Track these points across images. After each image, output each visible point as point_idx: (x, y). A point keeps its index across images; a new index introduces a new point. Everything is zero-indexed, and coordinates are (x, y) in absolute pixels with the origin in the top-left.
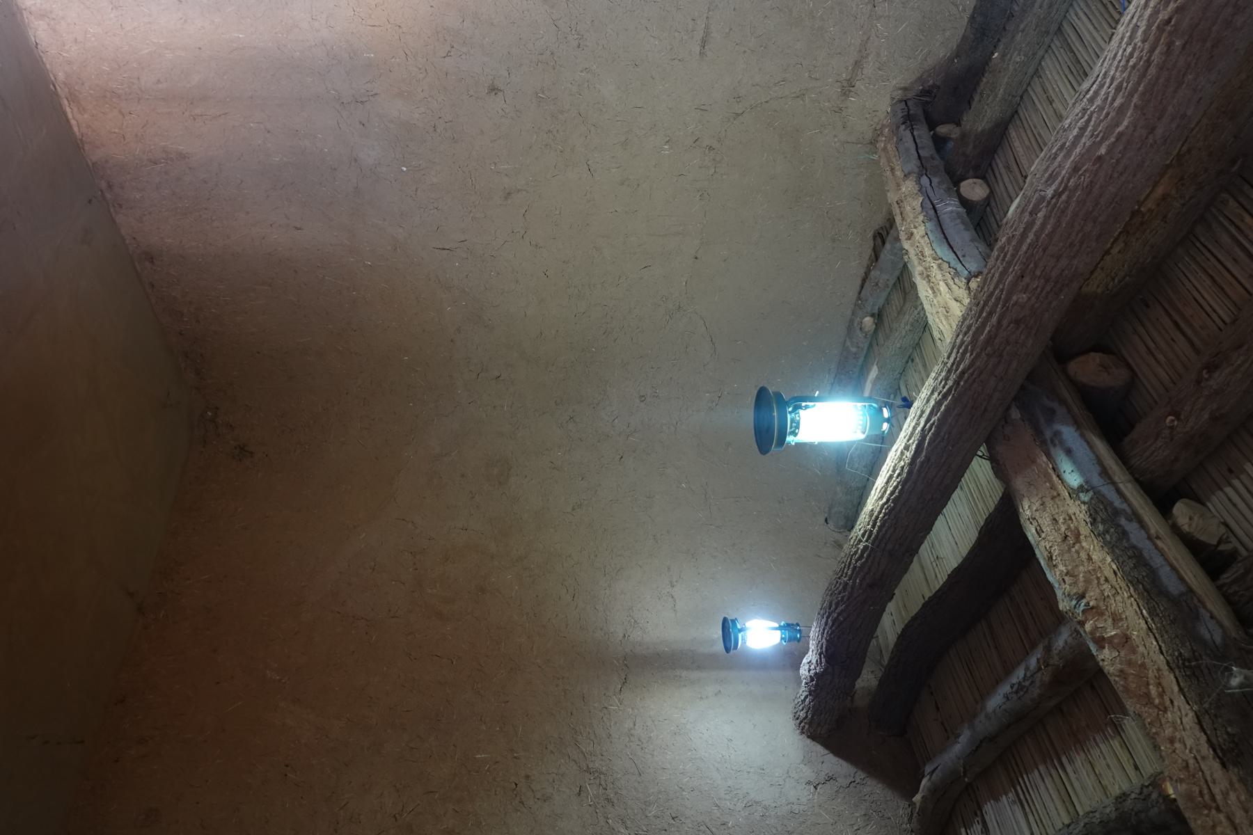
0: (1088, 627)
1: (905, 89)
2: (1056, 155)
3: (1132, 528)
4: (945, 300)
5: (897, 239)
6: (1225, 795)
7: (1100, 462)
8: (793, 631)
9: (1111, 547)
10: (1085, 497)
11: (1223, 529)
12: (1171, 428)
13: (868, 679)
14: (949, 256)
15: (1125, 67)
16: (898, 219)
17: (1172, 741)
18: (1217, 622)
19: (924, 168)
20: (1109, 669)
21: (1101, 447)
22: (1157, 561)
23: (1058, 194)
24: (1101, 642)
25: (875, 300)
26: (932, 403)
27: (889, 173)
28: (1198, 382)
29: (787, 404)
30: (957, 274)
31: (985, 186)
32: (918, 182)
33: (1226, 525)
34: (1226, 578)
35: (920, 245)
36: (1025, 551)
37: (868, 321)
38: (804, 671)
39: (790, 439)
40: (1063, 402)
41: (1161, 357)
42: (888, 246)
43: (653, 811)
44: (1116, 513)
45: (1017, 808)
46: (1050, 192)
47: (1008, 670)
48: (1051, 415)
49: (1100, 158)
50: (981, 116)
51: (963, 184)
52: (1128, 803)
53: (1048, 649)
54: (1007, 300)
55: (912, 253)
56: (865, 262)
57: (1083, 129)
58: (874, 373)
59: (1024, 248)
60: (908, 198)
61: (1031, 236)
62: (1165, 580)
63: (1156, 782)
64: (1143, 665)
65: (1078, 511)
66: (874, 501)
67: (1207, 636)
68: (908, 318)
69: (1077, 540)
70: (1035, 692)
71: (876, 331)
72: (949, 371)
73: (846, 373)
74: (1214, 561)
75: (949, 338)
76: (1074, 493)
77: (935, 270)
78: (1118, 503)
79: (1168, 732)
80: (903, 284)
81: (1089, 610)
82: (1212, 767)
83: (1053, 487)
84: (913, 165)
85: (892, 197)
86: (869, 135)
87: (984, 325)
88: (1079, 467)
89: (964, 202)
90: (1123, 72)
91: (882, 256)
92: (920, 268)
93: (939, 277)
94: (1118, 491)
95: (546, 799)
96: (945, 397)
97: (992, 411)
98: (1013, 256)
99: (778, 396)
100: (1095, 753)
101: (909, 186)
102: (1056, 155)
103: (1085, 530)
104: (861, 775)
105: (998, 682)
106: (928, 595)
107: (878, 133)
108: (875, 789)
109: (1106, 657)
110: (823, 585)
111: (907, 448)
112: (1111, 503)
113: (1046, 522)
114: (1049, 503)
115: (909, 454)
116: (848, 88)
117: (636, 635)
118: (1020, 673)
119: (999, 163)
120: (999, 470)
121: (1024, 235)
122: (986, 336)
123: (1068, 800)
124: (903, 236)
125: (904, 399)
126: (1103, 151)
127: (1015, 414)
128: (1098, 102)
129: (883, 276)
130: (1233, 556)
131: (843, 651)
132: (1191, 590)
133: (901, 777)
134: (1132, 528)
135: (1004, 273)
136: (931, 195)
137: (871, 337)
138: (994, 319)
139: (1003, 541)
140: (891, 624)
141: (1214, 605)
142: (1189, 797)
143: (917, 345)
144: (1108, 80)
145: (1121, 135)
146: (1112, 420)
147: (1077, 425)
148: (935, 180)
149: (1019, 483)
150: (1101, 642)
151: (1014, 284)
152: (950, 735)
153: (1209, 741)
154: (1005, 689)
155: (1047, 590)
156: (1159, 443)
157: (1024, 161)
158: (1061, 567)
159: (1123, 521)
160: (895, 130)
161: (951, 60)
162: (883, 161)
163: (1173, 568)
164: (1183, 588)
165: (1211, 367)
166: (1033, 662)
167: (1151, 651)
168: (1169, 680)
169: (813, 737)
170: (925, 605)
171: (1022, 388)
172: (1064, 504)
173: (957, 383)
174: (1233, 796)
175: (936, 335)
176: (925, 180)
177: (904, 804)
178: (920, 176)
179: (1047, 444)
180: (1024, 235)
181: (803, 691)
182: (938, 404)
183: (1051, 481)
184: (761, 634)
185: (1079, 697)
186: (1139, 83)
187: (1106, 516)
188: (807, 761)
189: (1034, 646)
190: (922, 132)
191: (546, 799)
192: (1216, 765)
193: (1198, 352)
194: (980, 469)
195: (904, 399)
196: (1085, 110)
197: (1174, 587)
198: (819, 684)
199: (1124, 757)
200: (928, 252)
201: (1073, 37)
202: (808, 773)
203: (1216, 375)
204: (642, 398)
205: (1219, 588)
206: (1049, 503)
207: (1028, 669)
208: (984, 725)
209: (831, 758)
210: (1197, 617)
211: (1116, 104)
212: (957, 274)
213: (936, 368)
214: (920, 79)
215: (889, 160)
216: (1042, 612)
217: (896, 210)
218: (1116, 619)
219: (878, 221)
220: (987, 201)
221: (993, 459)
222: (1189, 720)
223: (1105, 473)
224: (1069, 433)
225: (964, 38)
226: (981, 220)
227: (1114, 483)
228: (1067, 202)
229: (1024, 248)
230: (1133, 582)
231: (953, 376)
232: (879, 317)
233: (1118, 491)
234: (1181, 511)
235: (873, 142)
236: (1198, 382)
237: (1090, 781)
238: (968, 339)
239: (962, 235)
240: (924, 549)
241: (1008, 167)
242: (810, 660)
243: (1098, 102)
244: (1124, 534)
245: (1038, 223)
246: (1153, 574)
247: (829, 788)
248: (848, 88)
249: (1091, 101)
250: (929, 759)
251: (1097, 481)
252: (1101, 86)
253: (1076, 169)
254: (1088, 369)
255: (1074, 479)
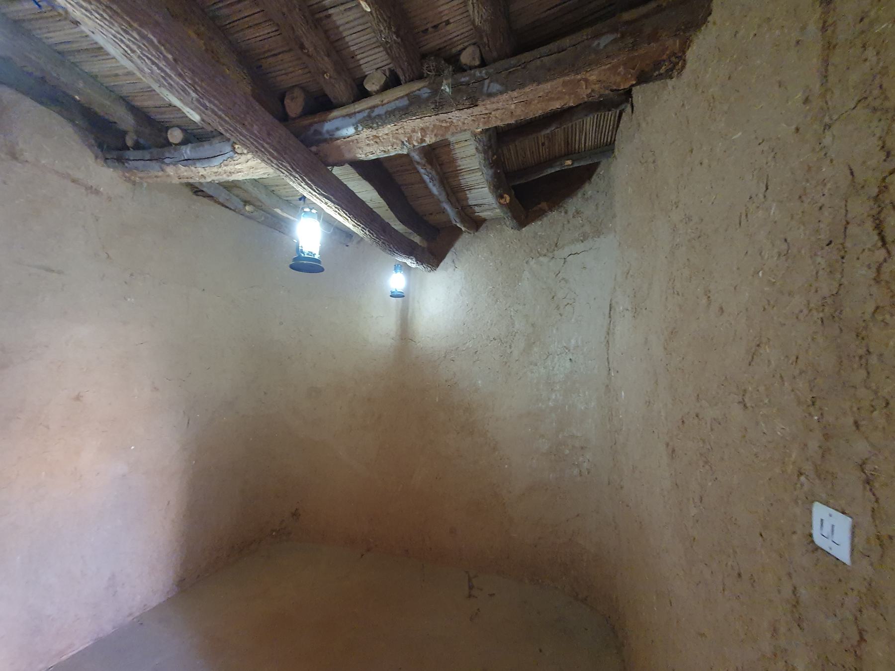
0: (416, 144)
1: (96, 157)
2: (169, 84)
3: (377, 112)
4: (247, 166)
5: (201, 183)
6: (486, 109)
7: (344, 116)
8: (396, 268)
9: (384, 124)
10: (360, 128)
11: (379, 71)
12: (330, 77)
13: (417, 239)
14: (219, 160)
15: (112, 23)
16: (191, 181)
17: (464, 123)
18: (420, 88)
19: (160, 159)
20: (433, 140)
21: (335, 113)
22: (393, 106)
23: (196, 91)
24: (423, 141)
25: (236, 202)
26: (306, 187)
27: (159, 179)
28: (309, 56)
29: (300, 256)
30: (232, 157)
31: (174, 129)
32: (168, 165)
33: (377, 69)
34: (402, 78)
35: (209, 173)
36: (377, 162)
37: (247, 208)
38: (414, 266)
39: (317, 257)
40: (311, 125)
41: (291, 69)
42: (204, 189)
43: (461, 332)
44: (369, 116)
45: (473, 191)
46: (194, 95)
47: (424, 182)
48: (317, 132)
49: (175, 60)
50: (126, 121)
51: (171, 140)
52: (480, 148)
53: (418, 163)
54: (256, 136)
55: (214, 178)
56: (212, 203)
57: (153, 63)
58: (278, 211)
59: (227, 119)
60: (176, 173)
61: (220, 113)
62: (401, 105)
63: (475, 135)
64: (434, 126)
65: (366, 133)
66: (349, 224)
67: (427, 95)
68: (250, 188)
69: (378, 137)
70: (434, 173)
71: (254, 205)
72: (291, 175)
73: (279, 226)
74: (393, 82)
75: (270, 170)
76: (357, 133)
77: (228, 169)
78: (365, 114)
79: (460, 123)
80: (230, 186)
81: (409, 141)
82: (476, 111)
83: (353, 141)
84: (155, 164)
85: (176, 181)
86: (130, 185)
87: (269, 152)
88: (347, 126)
89: (185, 142)
90: (113, 25)
91: (211, 194)
92: (225, 176)
93: (232, 167)
94: (359, 112)
95: (455, 374)
96: (304, 180)
97: (313, 158)
98: (231, 126)
99: (295, 259)
100: (458, 155)
101: (170, 170)
102: (169, 84)
103: (374, 133)
104: (452, 249)
105: (427, 187)
106: (387, 207)
107: (128, 180)
108: (458, 245)
109: (429, 140)
110: (378, 250)
111: (326, 203)
112: (364, 117)
113: (368, 149)
114: (359, 145)
115: (330, 203)
116: (93, 191)
117: (393, 334)
118: (426, 177)
119: (158, 117)
120: (340, 164)
121: (220, 117)
122: (279, 154)
123: (473, 171)
124: (203, 180)
125: (300, 199)
126: (170, 57)
127: (314, 149)
128: (134, 47)
129: (223, 196)
130: (392, 72)
131: (410, 250)
132: (407, 95)
133: (455, 233)
134: (377, 112)
135: (241, 134)
136: (177, 160)
137: (254, 208)
138: (265, 145)
139: (373, 171)
140: (398, 226)
141: (416, 86)
142: (485, 123)
143: (266, 187)
144: (119, 36)
145: (159, 42)
146: (322, 105)
147: (325, 121)
148: (167, 155)
149: (348, 156)
150: (423, 141)
151: (248, 130)
152: (444, 211)
153: (467, 108)
154: (431, 185)
155: (389, 159)
156: (337, 86)
157: (159, 103)
158: (389, 148)
159: (373, 115)
160: (130, 170)
161: (75, 125)
162: (150, 181)
163: (397, 99)
164: (406, 98)
165: (302, 47)
166: (422, 171)
167: (430, 121)
168: (442, 116)
169: (438, 266)
170: (392, 210)
171: (302, 141)
172: (367, 137)
173: (297, 173)
174: (488, 106)
175: (265, 176)
176: (167, 161)
177: (464, 235)
178: (163, 163)
179: (331, 139)
180: (220, 117)
181: (421, 267)
182: (307, 184)
183: (349, 142)
184: (397, 281)
185: (437, 155)
186: (123, 18)
187: (370, 121)
188: (446, 269)
189: (415, 169)
190: (131, 154)
191: (455, 374)
192: (476, 108)
193: (290, 50)
194: (336, 171)
195: (300, 199)
196: (139, 57)
197: (405, 102)
198: (420, 260)
199: (463, 144)
200: (215, 170)
201: (68, 46)
202: (451, 270)
203: (307, 46)
204: (281, 323)
205: (406, 82)
206: (359, 145)
207: (426, 174)
208: (443, 197)
209: (446, 260)
210: (419, 97)
211: (137, 37)
212: (232, 157)
213: (288, 181)
214: (90, 146)
215: (150, 177)
216: (403, 160)
217: (186, 180)
218: (414, 131)
219: (188, 192)
220: (184, 130)
221: (333, 166)
222: (457, 113)
223: (350, 115)
224: (328, 126)
225: (60, 113)
226: (196, 136)
227: (355, 113)
228: (201, 87)
229: (227, 119)
230: (401, 119)
231: (294, 173)
232: (246, 202)
233: (359, 112)
234: (370, 87)
235: (134, 183)
236: (309, 56)
237: (468, 160)
238: (275, 162)
239: (206, 149)
240: (371, 205)
241: (162, 113)
242: (411, 262)
243: (134, 47)
244: (379, 116)
245: (213, 107)
246: (398, 109)
247: (457, 262)
248: (93, 191)
249: (133, 51)
250: (450, 221)
251: (353, 120)
252: (122, 41)
253: (180, 75)
254: (294, 106)
255: (351, 131)
